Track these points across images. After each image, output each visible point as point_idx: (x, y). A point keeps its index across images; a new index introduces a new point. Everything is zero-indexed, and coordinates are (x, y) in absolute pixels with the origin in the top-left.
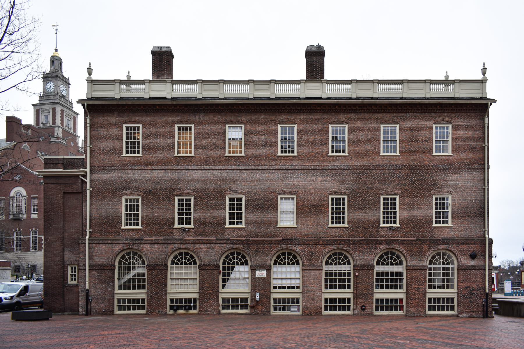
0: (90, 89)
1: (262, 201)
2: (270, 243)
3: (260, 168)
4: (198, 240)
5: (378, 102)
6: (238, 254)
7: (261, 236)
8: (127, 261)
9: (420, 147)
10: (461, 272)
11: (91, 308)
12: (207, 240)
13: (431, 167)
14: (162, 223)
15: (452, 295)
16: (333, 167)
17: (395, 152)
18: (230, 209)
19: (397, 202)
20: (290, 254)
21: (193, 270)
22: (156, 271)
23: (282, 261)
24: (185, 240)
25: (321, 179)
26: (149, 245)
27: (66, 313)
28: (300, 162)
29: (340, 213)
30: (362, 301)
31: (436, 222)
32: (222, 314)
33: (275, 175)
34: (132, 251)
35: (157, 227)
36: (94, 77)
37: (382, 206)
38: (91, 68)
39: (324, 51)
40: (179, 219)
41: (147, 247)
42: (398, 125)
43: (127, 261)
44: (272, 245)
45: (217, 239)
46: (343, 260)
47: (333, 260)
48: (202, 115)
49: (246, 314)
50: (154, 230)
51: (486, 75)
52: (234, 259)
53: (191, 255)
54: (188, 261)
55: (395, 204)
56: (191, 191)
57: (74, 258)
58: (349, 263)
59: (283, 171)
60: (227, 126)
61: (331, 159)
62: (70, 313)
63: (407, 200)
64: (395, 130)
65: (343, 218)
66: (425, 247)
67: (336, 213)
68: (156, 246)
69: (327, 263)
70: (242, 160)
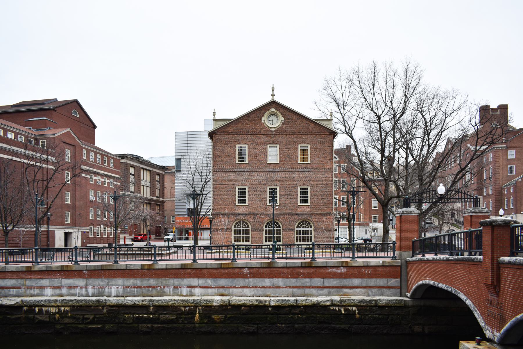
0: (214, 125)
6: (243, 222)
8: (307, 226)
10: (284, 233)
17: (307, 161)
18: (239, 194)
19: (309, 190)
20: (306, 222)
21: (488, 229)
23: (239, 226)
29: (305, 197)
31: (301, 202)
34: (241, 220)
36: (217, 117)
37: (268, 193)
40: (239, 200)
42: (247, 146)
43: (307, 226)
46: (307, 225)
47: (301, 225)
52: (303, 225)
53: (309, 222)
54: (244, 226)
55: (245, 192)
58: (311, 227)
60: (268, 146)
64: (246, 148)
65: (245, 200)
67: (303, 197)
69: (297, 227)
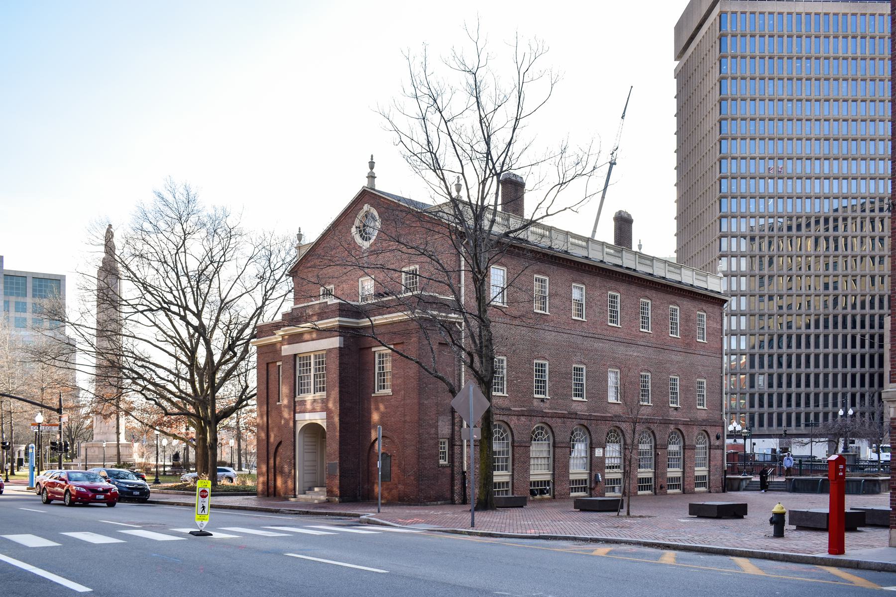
1: (597, 374)
2: (604, 419)
3: (597, 336)
4: (555, 413)
5: (669, 283)
7: (598, 412)
9: (690, 332)
11: (629, 492)
12: (562, 414)
13: (696, 352)
14: (525, 390)
15: (546, 477)
16: (643, 343)
22: (522, 448)
24: (545, 412)
25: (635, 354)
26: (516, 417)
27: (439, 503)
28: (622, 334)
30: (661, 480)
32: (639, 495)
33: (607, 346)
35: (520, 395)
38: (373, 160)
39: (629, 215)
41: (514, 418)
44: (607, 422)
45: (569, 413)
48: (555, 268)
49: (649, 495)
50: (518, 398)
51: (373, 171)
56: (547, 357)
57: (447, 430)
59: (612, 342)
61: (641, 334)
62: (443, 502)
63: (684, 383)
66: (695, 427)
68: (522, 417)
70: (584, 325)
